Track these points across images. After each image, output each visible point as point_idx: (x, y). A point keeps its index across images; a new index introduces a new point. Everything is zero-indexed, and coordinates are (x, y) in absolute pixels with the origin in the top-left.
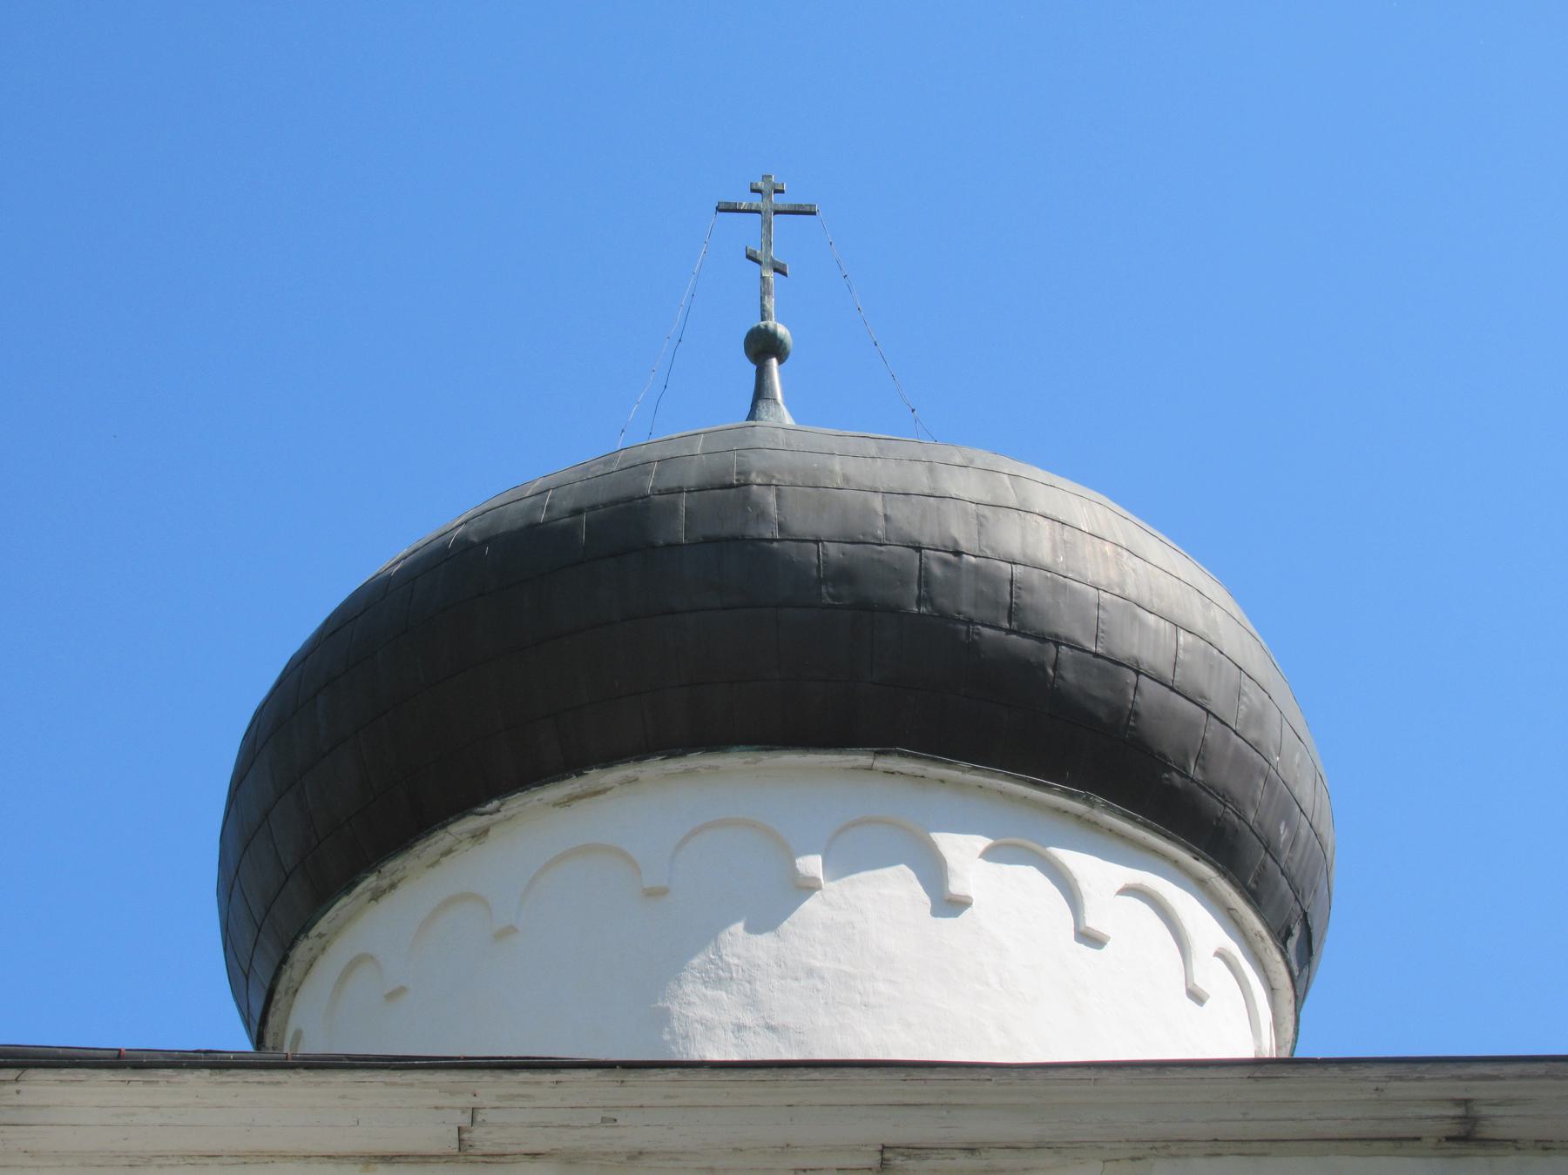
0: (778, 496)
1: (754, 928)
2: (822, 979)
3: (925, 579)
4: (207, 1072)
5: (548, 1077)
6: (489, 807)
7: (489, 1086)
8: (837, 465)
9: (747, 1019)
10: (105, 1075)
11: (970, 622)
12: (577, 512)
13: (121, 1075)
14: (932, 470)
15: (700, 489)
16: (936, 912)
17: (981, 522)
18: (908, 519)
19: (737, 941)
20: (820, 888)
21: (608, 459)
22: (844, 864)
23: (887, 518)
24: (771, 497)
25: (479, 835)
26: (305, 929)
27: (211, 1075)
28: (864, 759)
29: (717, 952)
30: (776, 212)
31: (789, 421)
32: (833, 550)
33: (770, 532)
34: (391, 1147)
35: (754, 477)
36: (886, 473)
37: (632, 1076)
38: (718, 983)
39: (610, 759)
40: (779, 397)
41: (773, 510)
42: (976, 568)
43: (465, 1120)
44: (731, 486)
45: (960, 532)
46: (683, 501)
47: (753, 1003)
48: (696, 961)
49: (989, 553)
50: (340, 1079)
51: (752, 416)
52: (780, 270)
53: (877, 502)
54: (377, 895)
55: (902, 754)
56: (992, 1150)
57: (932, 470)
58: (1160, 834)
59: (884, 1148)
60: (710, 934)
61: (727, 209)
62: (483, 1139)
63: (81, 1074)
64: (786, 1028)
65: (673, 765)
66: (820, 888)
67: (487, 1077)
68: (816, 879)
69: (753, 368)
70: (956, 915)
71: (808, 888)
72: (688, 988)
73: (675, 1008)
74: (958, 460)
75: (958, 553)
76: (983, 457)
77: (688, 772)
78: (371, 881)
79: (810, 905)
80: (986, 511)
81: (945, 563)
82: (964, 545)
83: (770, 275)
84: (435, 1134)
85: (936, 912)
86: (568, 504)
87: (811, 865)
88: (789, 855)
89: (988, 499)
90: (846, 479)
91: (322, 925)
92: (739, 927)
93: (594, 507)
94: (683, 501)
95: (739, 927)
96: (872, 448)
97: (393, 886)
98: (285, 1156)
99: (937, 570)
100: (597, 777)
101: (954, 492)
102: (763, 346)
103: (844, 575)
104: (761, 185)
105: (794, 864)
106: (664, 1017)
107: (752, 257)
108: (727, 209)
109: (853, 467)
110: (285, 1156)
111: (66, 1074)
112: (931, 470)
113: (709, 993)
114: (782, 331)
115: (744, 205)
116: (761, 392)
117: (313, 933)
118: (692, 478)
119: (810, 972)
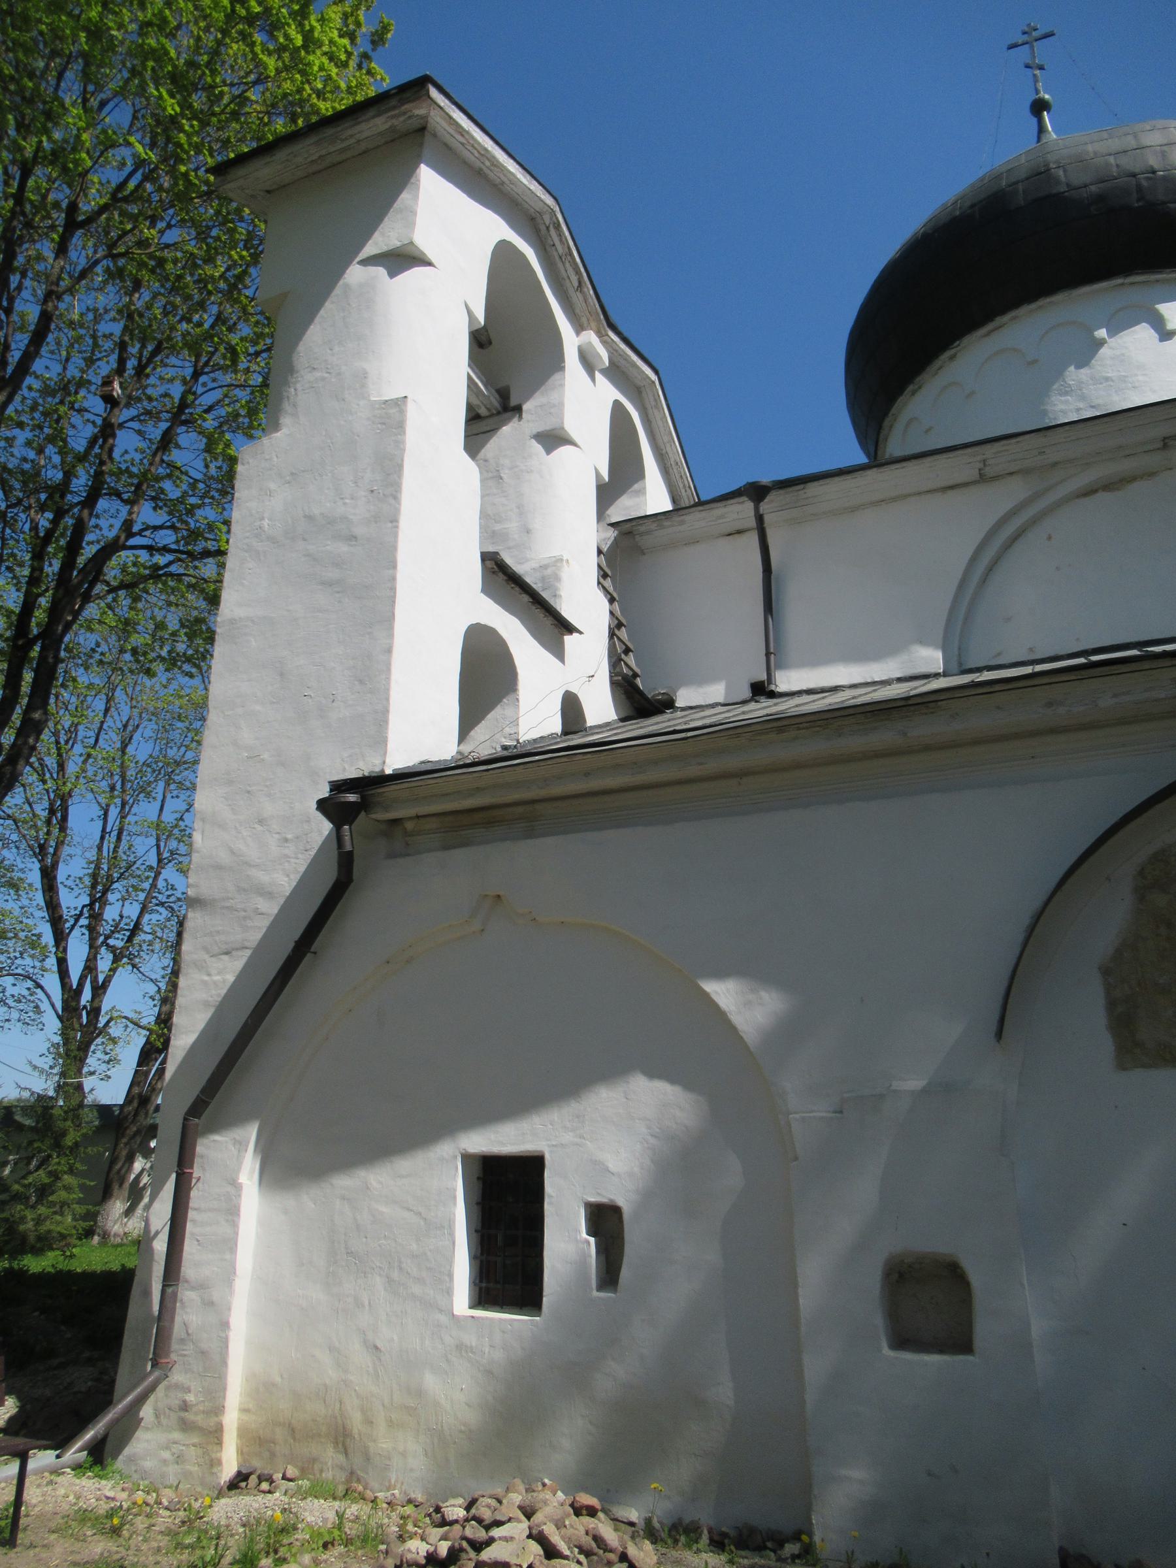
0: (1065, 171)
1: (1079, 366)
2: (1113, 381)
3: (1139, 188)
4: (875, 469)
5: (1013, 441)
6: (955, 344)
7: (989, 451)
8: (1090, 148)
9: (1081, 405)
10: (837, 479)
11: (1164, 203)
12: (972, 206)
13: (843, 477)
14: (1135, 136)
15: (1027, 179)
16: (1161, 340)
17: (1163, 154)
18: (1128, 163)
19: (1073, 375)
20: (1106, 342)
21: (982, 179)
22: (1114, 331)
23: (1118, 166)
24: (1061, 172)
25: (952, 358)
26: (886, 414)
27: (383, 771)
28: (1119, 281)
29: (1064, 380)
30: (1036, 40)
31: (1055, 137)
32: (1093, 188)
33: (1063, 188)
34: (951, 483)
35: (1052, 165)
36: (1115, 144)
37: (1049, 433)
38: (1066, 393)
39: (1003, 311)
40: (1050, 129)
41: (1063, 179)
42: (1163, 176)
43: (981, 465)
44: (1042, 173)
45: (1153, 161)
46: (1020, 187)
47: (1083, 398)
48: (1055, 387)
49: (1169, 168)
50: (928, 461)
51: (1039, 139)
52: (1041, 68)
53: (1112, 160)
54: (914, 393)
55: (1137, 274)
56: (190, 1332)
57: (1135, 136)
58: (455, 847)
59: (1165, 438)
60: (1059, 373)
61: (1011, 47)
62: (989, 472)
63: (828, 481)
64: (1099, 405)
65: (1033, 306)
66: (1106, 342)
67: (988, 446)
68: (1104, 339)
69: (1034, 120)
70: (1170, 339)
71: (1101, 343)
72: (1053, 399)
73: (1049, 408)
74: (1148, 128)
75: (1154, 172)
76: (1160, 123)
77: (1040, 307)
78: (911, 388)
79: (1103, 351)
80: (1165, 148)
81: (1148, 179)
82: (1156, 167)
83: (1037, 72)
84: (970, 473)
85: (1161, 340)
86: (968, 203)
87: (1102, 333)
88: (1090, 331)
89: (1165, 142)
90: (1095, 153)
91: (893, 411)
92: (1072, 368)
93: (981, 201)
94: (1020, 187)
95: (1072, 368)
96: (1105, 135)
97: (920, 388)
98: (910, 495)
99: (1145, 183)
100: (999, 320)
101: (1149, 144)
102: (1039, 107)
103: (1100, 198)
104: (1026, 29)
105: (1093, 336)
106: (1045, 413)
107: (1027, 66)
108: (1011, 47)
109: (1101, 147)
110: (910, 495)
111: (821, 482)
112: (1135, 137)
113: (1063, 398)
114: (1047, 97)
115: (1020, 42)
116: (1041, 129)
117: (890, 415)
118: (1022, 174)
119: (1107, 379)
